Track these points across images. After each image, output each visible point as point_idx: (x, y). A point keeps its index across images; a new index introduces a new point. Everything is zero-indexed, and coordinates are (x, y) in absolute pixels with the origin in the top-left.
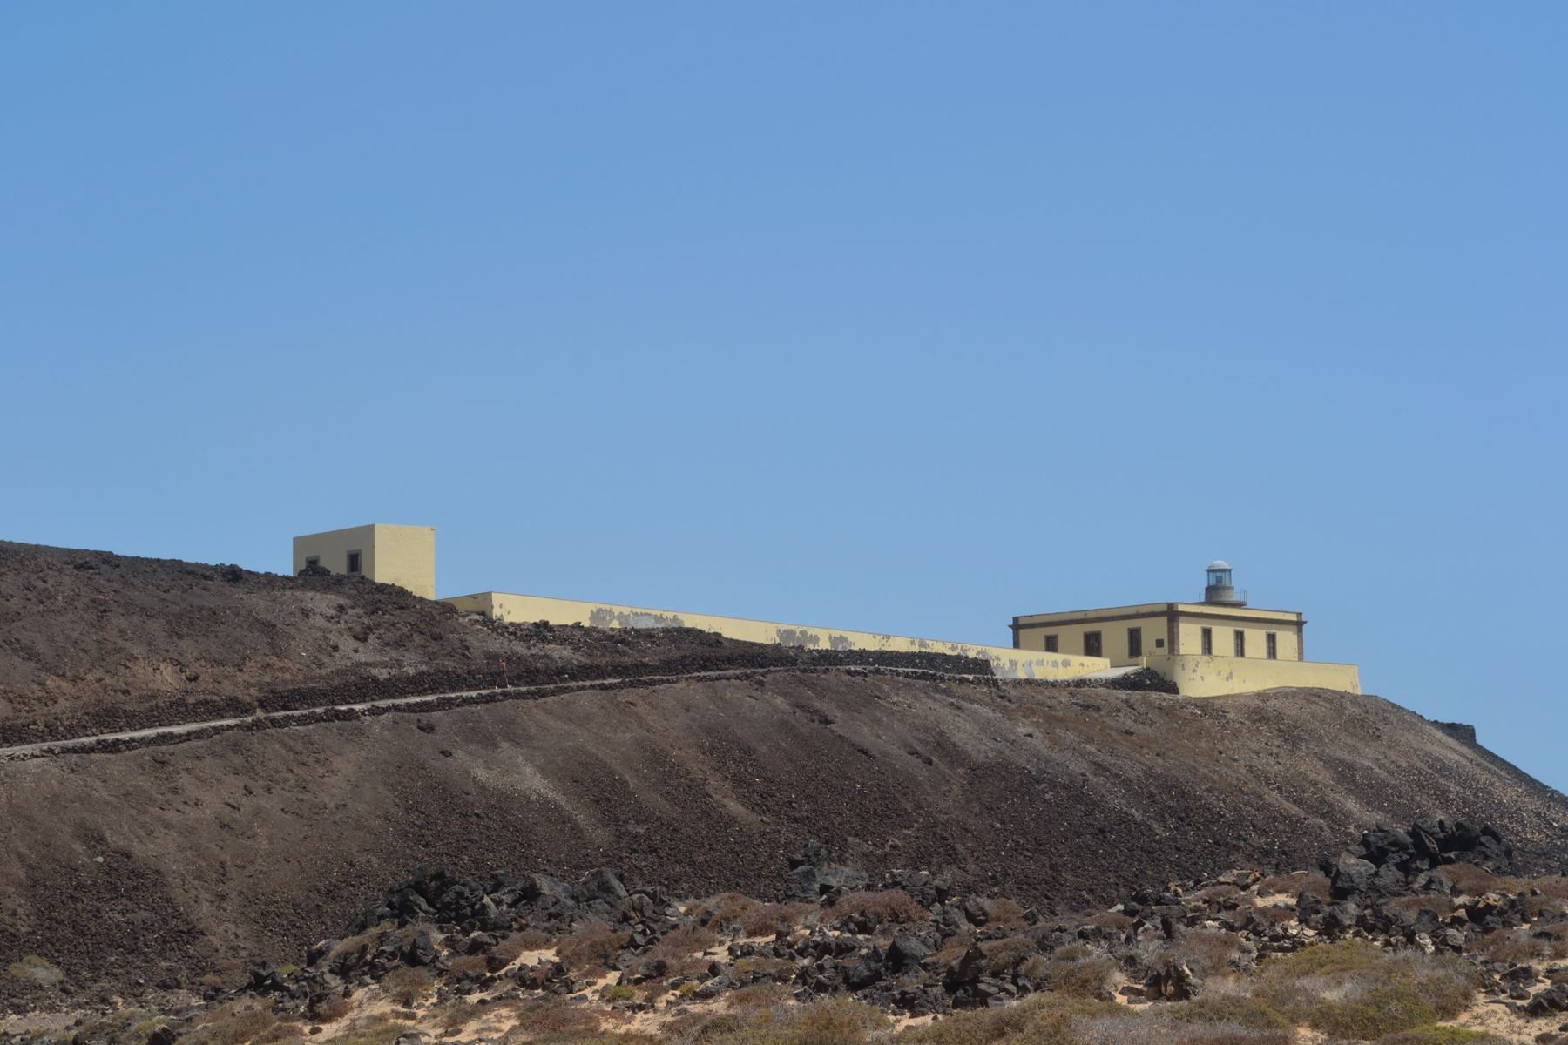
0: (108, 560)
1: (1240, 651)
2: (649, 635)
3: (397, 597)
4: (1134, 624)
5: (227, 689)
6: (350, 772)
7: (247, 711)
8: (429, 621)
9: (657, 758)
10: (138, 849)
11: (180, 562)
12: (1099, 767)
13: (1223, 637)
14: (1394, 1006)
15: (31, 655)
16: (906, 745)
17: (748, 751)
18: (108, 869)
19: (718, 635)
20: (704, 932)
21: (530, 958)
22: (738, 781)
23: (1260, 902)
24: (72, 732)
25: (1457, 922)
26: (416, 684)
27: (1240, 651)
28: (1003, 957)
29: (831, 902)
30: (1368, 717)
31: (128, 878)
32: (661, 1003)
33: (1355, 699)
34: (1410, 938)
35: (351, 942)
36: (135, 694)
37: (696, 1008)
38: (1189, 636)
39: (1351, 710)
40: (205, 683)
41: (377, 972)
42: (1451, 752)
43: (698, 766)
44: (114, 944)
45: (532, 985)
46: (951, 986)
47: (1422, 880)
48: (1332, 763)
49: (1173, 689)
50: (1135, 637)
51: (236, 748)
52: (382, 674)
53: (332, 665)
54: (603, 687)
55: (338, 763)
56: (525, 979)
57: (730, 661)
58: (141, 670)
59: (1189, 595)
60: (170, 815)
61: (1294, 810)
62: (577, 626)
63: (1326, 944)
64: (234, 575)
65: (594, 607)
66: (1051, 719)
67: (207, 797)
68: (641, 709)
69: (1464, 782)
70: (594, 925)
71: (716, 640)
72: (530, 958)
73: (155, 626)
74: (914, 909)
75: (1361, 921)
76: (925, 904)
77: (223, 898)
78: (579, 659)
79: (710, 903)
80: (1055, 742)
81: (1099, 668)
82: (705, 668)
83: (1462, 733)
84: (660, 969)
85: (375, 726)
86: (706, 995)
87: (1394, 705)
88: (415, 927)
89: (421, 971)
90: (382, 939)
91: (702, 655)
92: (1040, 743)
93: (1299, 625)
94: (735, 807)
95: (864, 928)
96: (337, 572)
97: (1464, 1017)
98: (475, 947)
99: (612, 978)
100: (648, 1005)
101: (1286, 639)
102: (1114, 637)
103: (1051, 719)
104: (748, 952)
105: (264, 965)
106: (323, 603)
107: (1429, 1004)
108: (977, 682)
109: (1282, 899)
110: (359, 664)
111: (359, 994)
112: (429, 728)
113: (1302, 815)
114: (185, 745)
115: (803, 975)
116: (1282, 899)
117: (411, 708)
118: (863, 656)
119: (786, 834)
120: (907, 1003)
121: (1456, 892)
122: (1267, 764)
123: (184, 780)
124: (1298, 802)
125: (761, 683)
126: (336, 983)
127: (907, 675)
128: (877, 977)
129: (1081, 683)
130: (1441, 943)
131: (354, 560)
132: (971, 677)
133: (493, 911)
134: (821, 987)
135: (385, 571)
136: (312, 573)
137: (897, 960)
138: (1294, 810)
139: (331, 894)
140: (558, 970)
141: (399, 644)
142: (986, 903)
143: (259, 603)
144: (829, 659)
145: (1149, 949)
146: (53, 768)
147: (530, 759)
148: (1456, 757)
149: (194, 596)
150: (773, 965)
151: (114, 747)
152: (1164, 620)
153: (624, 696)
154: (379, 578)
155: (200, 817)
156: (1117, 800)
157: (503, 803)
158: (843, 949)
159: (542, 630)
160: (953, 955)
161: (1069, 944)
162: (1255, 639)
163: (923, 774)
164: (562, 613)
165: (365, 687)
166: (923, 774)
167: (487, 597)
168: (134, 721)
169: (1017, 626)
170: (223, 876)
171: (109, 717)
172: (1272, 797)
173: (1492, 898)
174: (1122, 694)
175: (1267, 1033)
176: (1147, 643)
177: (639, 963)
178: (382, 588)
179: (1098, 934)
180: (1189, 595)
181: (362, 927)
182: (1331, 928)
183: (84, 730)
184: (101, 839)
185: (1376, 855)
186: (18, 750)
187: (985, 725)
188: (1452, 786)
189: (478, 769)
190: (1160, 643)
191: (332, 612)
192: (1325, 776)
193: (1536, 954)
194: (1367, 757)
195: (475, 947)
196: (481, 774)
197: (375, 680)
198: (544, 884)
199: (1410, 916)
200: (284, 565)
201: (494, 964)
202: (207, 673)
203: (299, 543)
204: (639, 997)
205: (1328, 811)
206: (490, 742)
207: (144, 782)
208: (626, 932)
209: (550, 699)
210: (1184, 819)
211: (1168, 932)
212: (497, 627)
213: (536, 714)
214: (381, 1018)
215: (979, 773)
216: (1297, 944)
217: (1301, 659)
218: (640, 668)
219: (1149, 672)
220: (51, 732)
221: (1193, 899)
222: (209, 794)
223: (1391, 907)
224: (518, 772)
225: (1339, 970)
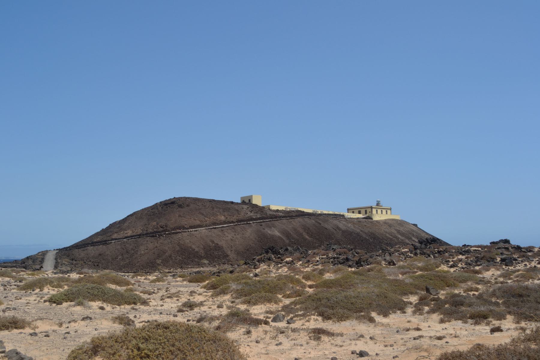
0: (214, 200)
1: (382, 213)
2: (293, 211)
3: (256, 206)
5: (232, 220)
6: (250, 232)
7: (234, 223)
8: (261, 209)
9: (295, 230)
10: (219, 243)
11: (257, 205)
12: (361, 231)
13: (379, 211)
14: (430, 266)
15: (203, 215)
17: (309, 228)
18: (215, 246)
20: (315, 255)
21: (288, 259)
22: (307, 233)
23: (403, 250)
24: (209, 226)
25: (436, 253)
26: (259, 219)
27: (382, 213)
28: (364, 259)
29: (334, 251)
30: (401, 223)
31: (218, 248)
32: (310, 266)
33: (399, 220)
34: (429, 256)
35: (259, 257)
37: (316, 267)
38: (374, 211)
39: (399, 222)
40: (228, 219)
41: (264, 261)
42: (414, 228)
43: (301, 231)
44: (216, 257)
45: (288, 263)
46: (357, 263)
47: (428, 247)
48: (396, 230)
49: (372, 219)
50: (366, 211)
51: (233, 228)
52: (254, 217)
53: (247, 216)
55: (248, 230)
56: (287, 263)
57: (306, 215)
58: (219, 217)
59: (374, 205)
60: (224, 238)
63: (415, 257)
64: (232, 203)
66: (354, 224)
67: (229, 236)
68: (293, 222)
69: (416, 233)
70: (297, 254)
71: (303, 212)
72: (288, 259)
73: (221, 210)
74: (348, 252)
75: (420, 253)
76: (349, 251)
78: (283, 215)
79: (315, 251)
80: (355, 227)
81: (361, 216)
83: (415, 225)
84: (309, 261)
85: (253, 225)
86: (317, 265)
88: (269, 255)
89: (271, 261)
90: (264, 256)
91: (301, 214)
92: (352, 227)
93: (391, 209)
94: (307, 237)
95: (340, 255)
96: (247, 202)
97: (440, 268)
98: (279, 258)
99: (301, 262)
100: (308, 267)
101: (389, 211)
102: (363, 211)
103: (354, 224)
104: (322, 258)
106: (245, 207)
107: (435, 266)
109: (406, 250)
111: (261, 265)
112: (261, 225)
115: (332, 262)
116: (406, 250)
118: (325, 214)
119: (315, 241)
120: (350, 266)
121: (434, 248)
122: (386, 230)
123: (226, 233)
126: (257, 263)
128: (344, 262)
129: (358, 218)
130: (435, 257)
131: (250, 200)
133: (281, 252)
134: (336, 264)
135: (254, 202)
136: (243, 202)
137: (347, 260)
139: (248, 250)
140: (292, 261)
141: (257, 213)
142: (358, 250)
143: (236, 207)
144: (320, 215)
145: (388, 258)
146: (207, 231)
149: (225, 206)
150: (327, 260)
151: (215, 228)
153: (290, 220)
154: (253, 203)
155: (229, 238)
156: (364, 236)
157: (273, 237)
158: (338, 258)
159: (278, 211)
160: (357, 259)
161: (375, 257)
162: (384, 211)
163: (335, 232)
164: (280, 208)
165: (252, 219)
166: (335, 232)
167: (269, 206)
168: (218, 224)
169: (348, 210)
170: (232, 248)
171: (215, 224)
172: (388, 235)
173: (441, 249)
177: (305, 261)
178: (254, 205)
179: (379, 256)
180: (374, 205)
181: (261, 255)
182: (416, 254)
183: (211, 226)
185: (421, 243)
186: (201, 229)
187: (344, 225)
189: (269, 232)
192: (395, 232)
193: (450, 258)
194: (401, 229)
195: (279, 258)
196: (269, 232)
198: (289, 248)
199: (428, 252)
200: (239, 201)
201: (282, 260)
202: (229, 217)
203: (241, 198)
204: (306, 265)
205: (396, 237)
206: (270, 227)
207: (220, 233)
208: (302, 255)
210: (374, 238)
211: (390, 255)
212: (269, 209)
213: (277, 223)
214: (265, 269)
215: (344, 232)
216: (411, 257)
218: (292, 216)
219: (368, 216)
220: (206, 226)
221: (392, 250)
222: (229, 235)
223: (425, 251)
224: (275, 231)
225: (420, 261)
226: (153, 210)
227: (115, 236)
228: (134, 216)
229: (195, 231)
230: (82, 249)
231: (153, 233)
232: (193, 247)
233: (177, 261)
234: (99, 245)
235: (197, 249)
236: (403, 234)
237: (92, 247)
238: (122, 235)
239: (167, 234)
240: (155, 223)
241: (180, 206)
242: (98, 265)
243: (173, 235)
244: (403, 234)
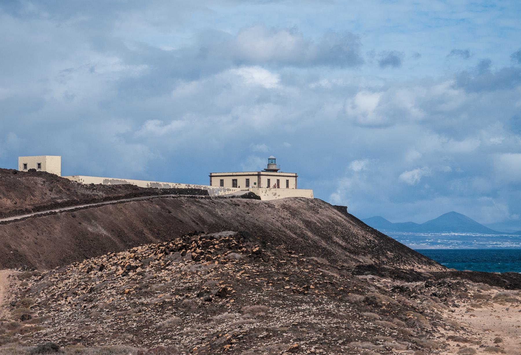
2: (118, 187)
4: (247, 177)
9: (131, 224)
16: (191, 219)
18: (14, 254)
19: (136, 186)
22: (151, 230)
36: (4, 208)
40: (18, 205)
43: (140, 226)
50: (248, 181)
51: (32, 222)
52: (59, 201)
54: (113, 204)
55: (56, 227)
57: (91, 201)
61: (294, 236)
62: (101, 184)
65: (104, 178)
71: (135, 188)
77: (41, 261)
82: (135, 196)
83: (342, 209)
87: (323, 201)
91: (134, 192)
101: (292, 181)
102: (242, 181)
108: (205, 198)
110: (52, 198)
112: (74, 216)
113: (296, 237)
114: (20, 222)
117: (69, 211)
124: (295, 233)
125: (152, 201)
127: (188, 197)
132: (204, 196)
138: (294, 236)
147: (100, 225)
148: (339, 218)
152: (257, 177)
153: (120, 206)
154: (19, 157)
159: (92, 186)
164: (98, 181)
174: (245, 200)
175: (39, 332)
176: (251, 184)
184: (10, 247)
188: (339, 228)
190: (255, 184)
191: (42, 183)
192: (301, 225)
196: (90, 229)
197: (58, 203)
205: (303, 236)
209: (101, 207)
217: (296, 188)
236: (316, 230)
244: (316, 230)
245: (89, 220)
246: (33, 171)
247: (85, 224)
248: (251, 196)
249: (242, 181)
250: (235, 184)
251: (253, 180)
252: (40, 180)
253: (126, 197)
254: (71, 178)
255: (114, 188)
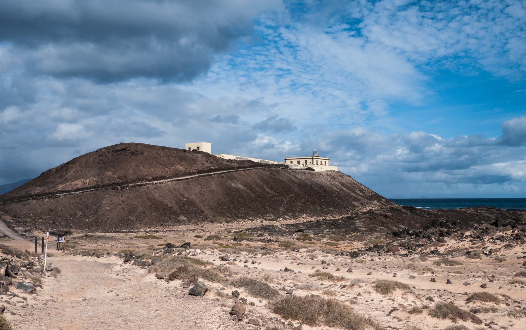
18: (187, 201)
22: (267, 186)
31: (190, 202)
40: (188, 169)
43: (261, 184)
50: (306, 161)
51: (197, 180)
55: (212, 183)
71: (253, 162)
91: (254, 165)
94: (268, 190)
102: (302, 161)
105: (522, 287)
112: (222, 177)
139: (220, 205)
143: (298, 171)
157: (238, 190)
164: (233, 157)
171: (177, 175)
176: (308, 163)
192: (339, 184)
194: (344, 181)
196: (233, 185)
220: (169, 178)
226: (101, 158)
227: (60, 187)
228: (77, 164)
229: (160, 183)
230: (21, 203)
231: (112, 185)
232: (166, 202)
233: (154, 217)
234: (43, 198)
235: (170, 205)
236: (347, 187)
237: (34, 201)
238: (68, 186)
239: (131, 186)
240: (110, 173)
241: (133, 154)
242: (54, 223)
243: (137, 188)
245: (232, 180)
246: (195, 150)
247: (229, 182)
248: (309, 169)
249: (302, 161)
250: (299, 163)
251: (309, 161)
252: (200, 156)
253: (250, 167)
254: (217, 156)
255: (242, 162)
